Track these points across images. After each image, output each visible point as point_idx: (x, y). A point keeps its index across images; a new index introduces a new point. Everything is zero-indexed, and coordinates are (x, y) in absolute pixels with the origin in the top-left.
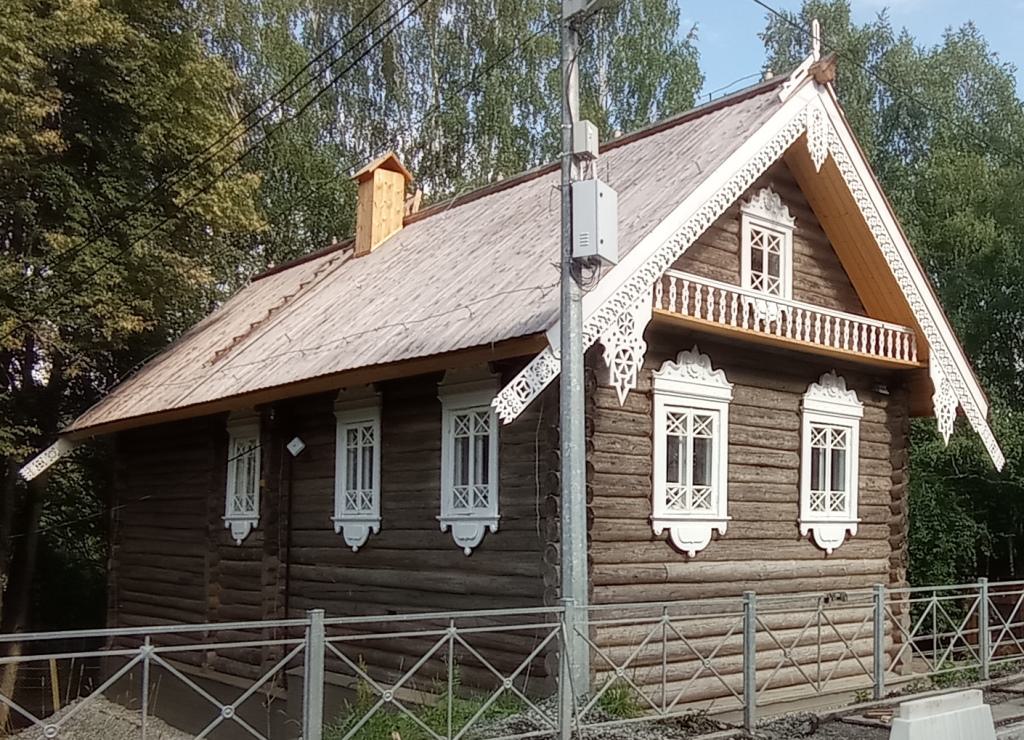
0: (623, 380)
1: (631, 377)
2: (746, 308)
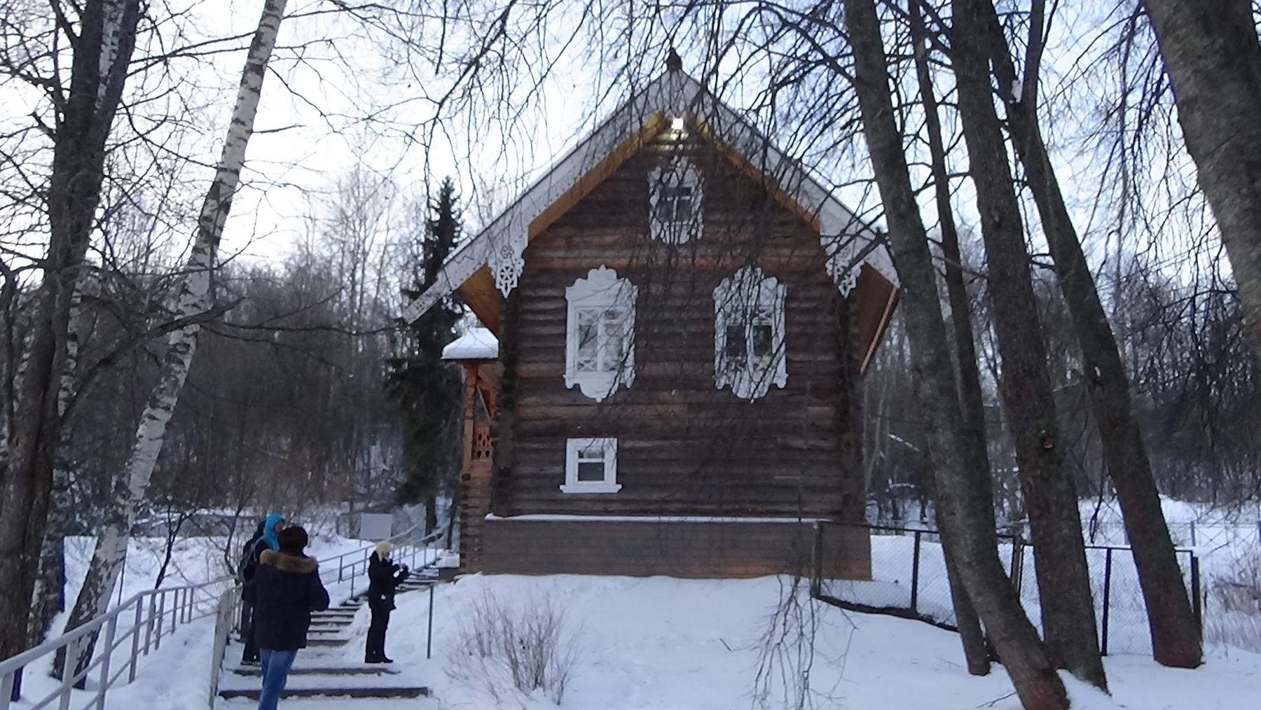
2: (350, 620)
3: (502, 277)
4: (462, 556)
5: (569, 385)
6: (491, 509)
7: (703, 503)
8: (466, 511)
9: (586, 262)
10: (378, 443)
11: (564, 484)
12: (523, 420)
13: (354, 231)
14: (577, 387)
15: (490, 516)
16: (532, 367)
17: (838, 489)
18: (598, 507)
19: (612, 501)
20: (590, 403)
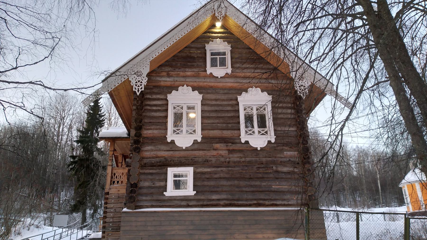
3: (136, 85)
4: (104, 232)
5: (169, 140)
6: (126, 205)
7: (238, 200)
8: (106, 210)
9: (177, 83)
10: (64, 190)
11: (166, 191)
12: (143, 158)
13: (60, 114)
14: (173, 142)
15: (125, 210)
16: (150, 132)
17: (305, 192)
18: (184, 203)
19: (191, 200)
20: (180, 149)
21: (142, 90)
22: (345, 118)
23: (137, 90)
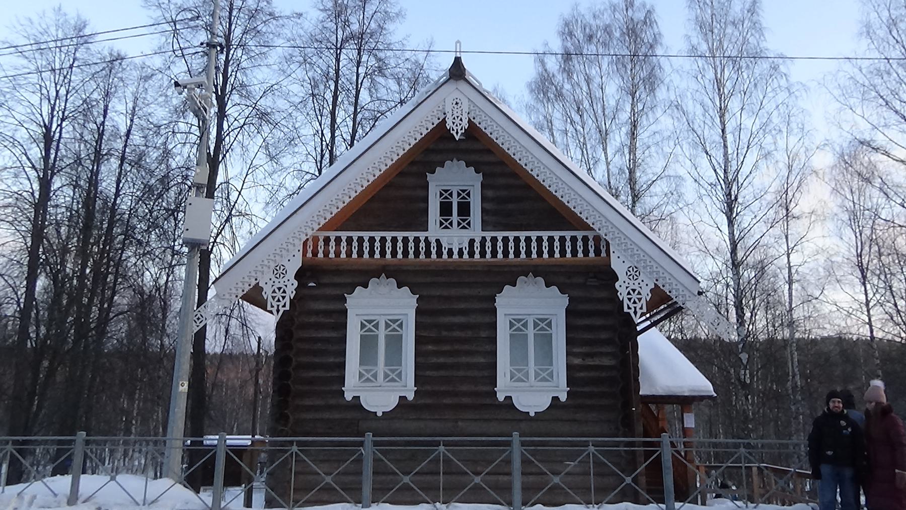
0: (278, 306)
1: (285, 304)
2: (434, 244)
21: (284, 309)
22: (639, 338)
23: (633, 309)
